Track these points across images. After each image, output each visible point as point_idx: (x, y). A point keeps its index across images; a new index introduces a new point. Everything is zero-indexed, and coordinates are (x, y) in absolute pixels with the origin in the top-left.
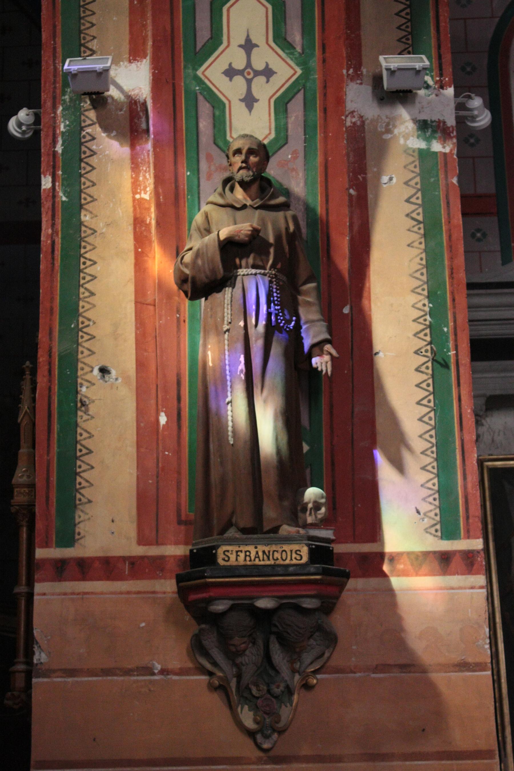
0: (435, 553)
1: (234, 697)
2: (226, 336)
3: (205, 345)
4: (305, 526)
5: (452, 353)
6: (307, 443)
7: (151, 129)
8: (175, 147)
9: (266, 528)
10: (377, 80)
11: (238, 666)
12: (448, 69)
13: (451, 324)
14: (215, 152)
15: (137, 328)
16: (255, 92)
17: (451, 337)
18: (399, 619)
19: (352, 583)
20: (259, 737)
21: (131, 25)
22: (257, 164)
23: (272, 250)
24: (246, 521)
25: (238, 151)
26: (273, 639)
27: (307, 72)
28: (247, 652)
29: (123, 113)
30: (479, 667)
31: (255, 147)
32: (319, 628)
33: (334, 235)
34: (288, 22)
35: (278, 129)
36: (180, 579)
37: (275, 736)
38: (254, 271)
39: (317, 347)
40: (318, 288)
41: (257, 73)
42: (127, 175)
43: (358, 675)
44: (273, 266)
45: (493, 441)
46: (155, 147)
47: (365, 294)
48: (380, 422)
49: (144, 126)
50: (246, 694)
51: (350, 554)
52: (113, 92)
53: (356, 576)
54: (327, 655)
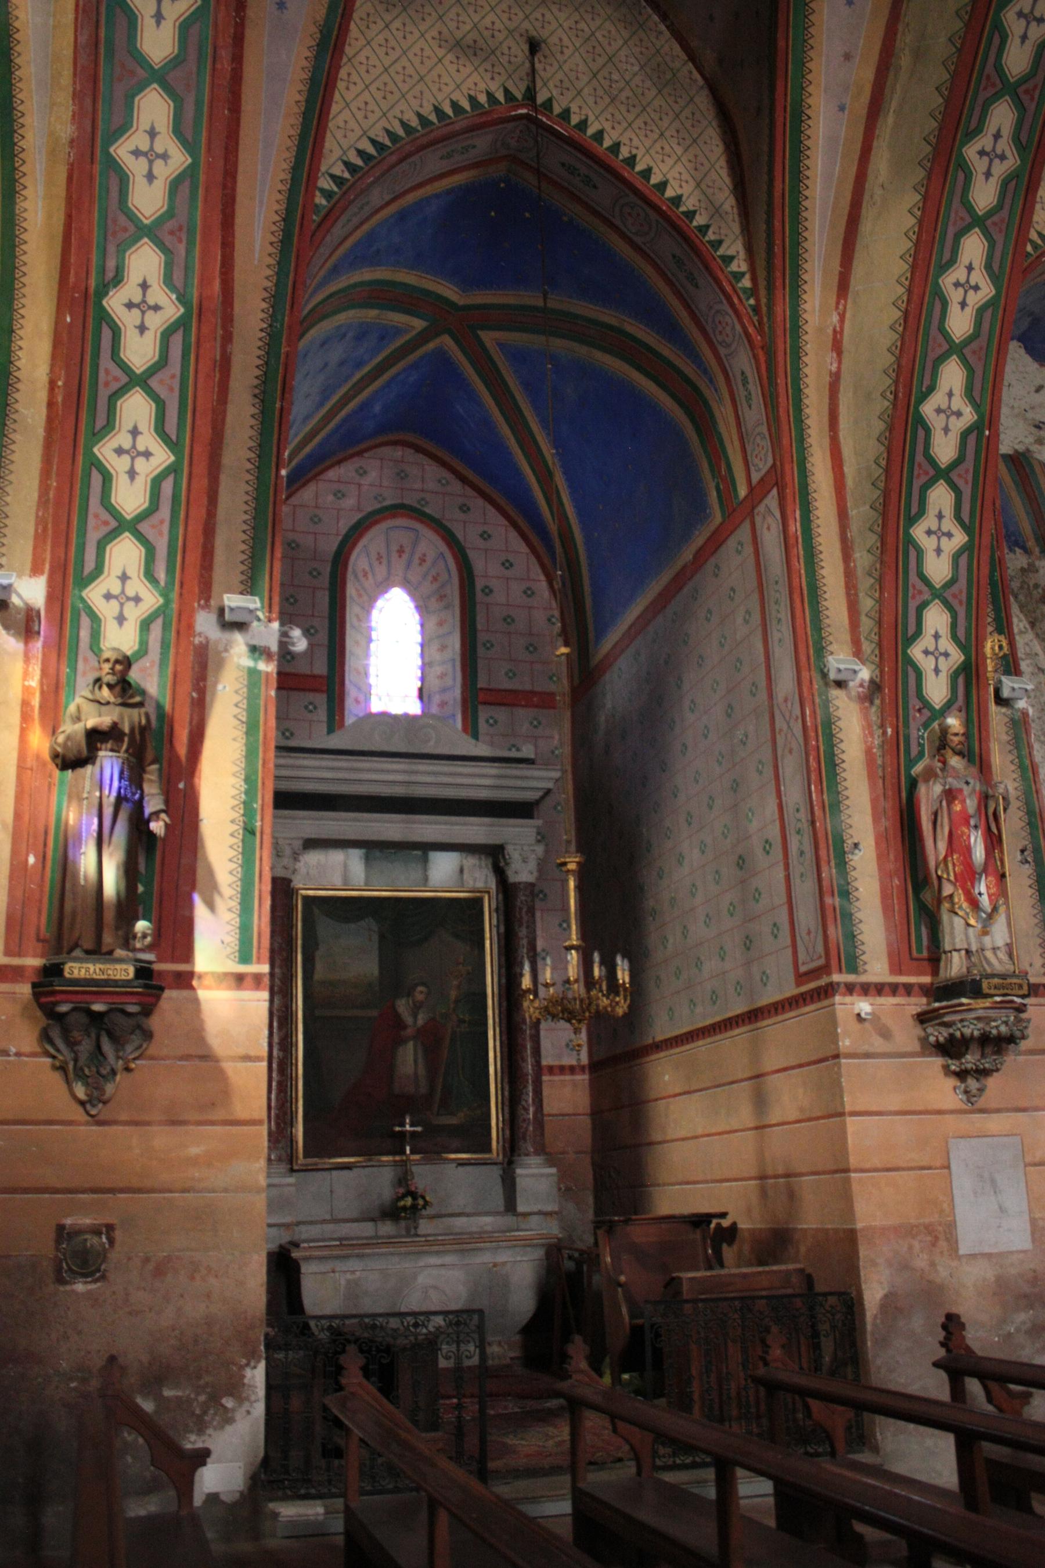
0: (232, 974)
1: (71, 1075)
2: (85, 802)
3: (68, 807)
4: (134, 950)
5: (258, 824)
6: (143, 885)
7: (42, 633)
8: (60, 649)
9: (104, 949)
10: (221, 611)
11: (76, 1053)
12: (276, 608)
13: (260, 802)
14: (90, 655)
15: (17, 786)
16: (126, 613)
17: (259, 812)
18: (202, 1022)
19: (167, 994)
20: (88, 1106)
21: (35, 548)
22: (121, 672)
23: (126, 739)
24: (88, 944)
25: (107, 660)
26: (103, 1033)
27: (167, 602)
28: (84, 1043)
29: (21, 616)
30: (258, 1059)
31: (120, 658)
32: (139, 1027)
33: (177, 727)
34: (156, 563)
35: (141, 643)
36: (34, 986)
37: (100, 1105)
38: (110, 754)
39: (156, 814)
40: (160, 770)
41: (128, 599)
42: (19, 666)
43: (167, 1062)
44: (127, 751)
45: (308, 873)
46: (44, 647)
47: (197, 774)
48: (200, 873)
49: (36, 628)
50: (81, 1074)
51: (168, 972)
52: (15, 600)
53: (171, 988)
54: (145, 1046)
